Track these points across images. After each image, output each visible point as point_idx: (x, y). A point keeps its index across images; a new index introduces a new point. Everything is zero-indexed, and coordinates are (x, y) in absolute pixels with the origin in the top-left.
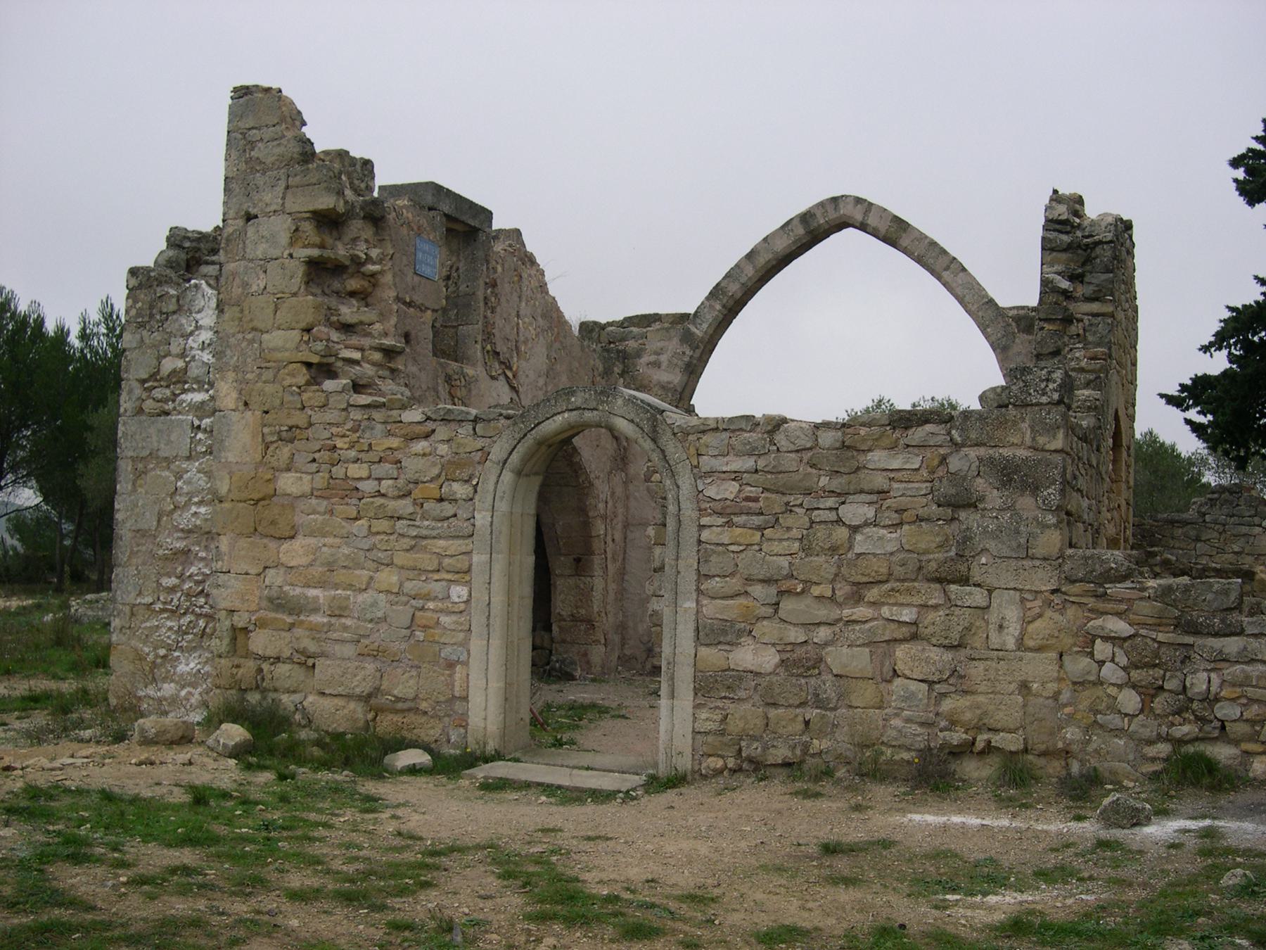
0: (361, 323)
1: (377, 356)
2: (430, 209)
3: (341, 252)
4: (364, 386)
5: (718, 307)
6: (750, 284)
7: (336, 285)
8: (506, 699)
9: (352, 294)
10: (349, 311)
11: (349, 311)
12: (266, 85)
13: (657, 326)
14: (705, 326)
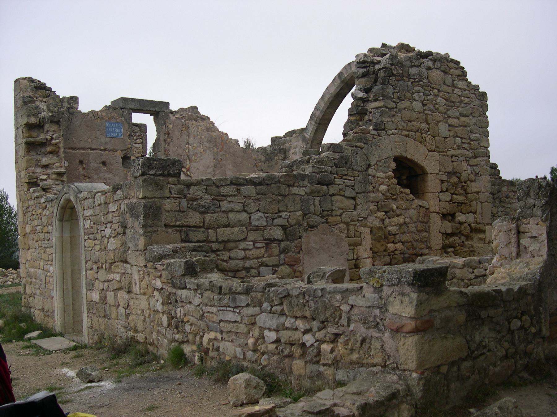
0: (50, 164)
1: (54, 176)
2: (121, 109)
3: (42, 137)
4: (48, 189)
5: (313, 123)
6: (324, 111)
7: (43, 150)
8: (65, 312)
9: (50, 153)
10: (45, 160)
11: (45, 160)
12: (24, 77)
13: (295, 135)
14: (310, 133)
